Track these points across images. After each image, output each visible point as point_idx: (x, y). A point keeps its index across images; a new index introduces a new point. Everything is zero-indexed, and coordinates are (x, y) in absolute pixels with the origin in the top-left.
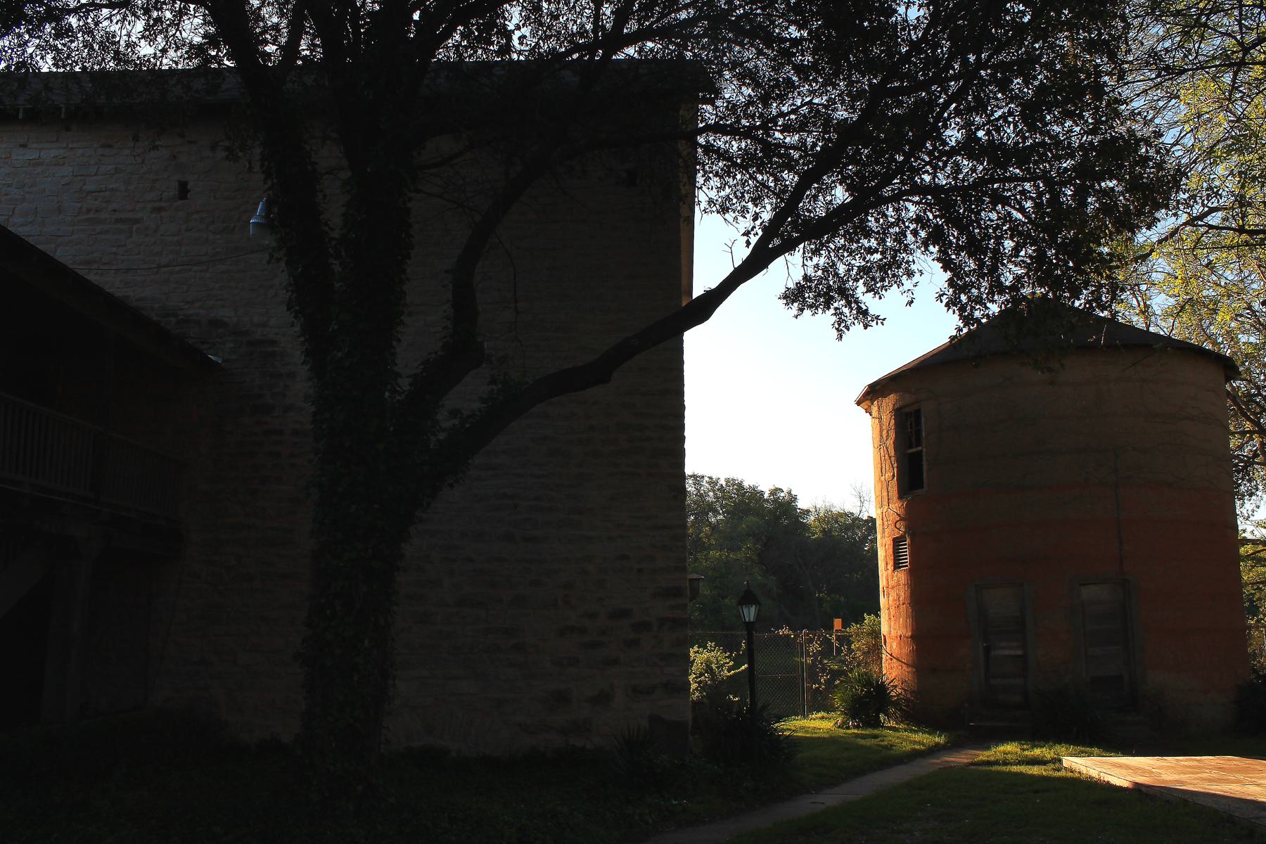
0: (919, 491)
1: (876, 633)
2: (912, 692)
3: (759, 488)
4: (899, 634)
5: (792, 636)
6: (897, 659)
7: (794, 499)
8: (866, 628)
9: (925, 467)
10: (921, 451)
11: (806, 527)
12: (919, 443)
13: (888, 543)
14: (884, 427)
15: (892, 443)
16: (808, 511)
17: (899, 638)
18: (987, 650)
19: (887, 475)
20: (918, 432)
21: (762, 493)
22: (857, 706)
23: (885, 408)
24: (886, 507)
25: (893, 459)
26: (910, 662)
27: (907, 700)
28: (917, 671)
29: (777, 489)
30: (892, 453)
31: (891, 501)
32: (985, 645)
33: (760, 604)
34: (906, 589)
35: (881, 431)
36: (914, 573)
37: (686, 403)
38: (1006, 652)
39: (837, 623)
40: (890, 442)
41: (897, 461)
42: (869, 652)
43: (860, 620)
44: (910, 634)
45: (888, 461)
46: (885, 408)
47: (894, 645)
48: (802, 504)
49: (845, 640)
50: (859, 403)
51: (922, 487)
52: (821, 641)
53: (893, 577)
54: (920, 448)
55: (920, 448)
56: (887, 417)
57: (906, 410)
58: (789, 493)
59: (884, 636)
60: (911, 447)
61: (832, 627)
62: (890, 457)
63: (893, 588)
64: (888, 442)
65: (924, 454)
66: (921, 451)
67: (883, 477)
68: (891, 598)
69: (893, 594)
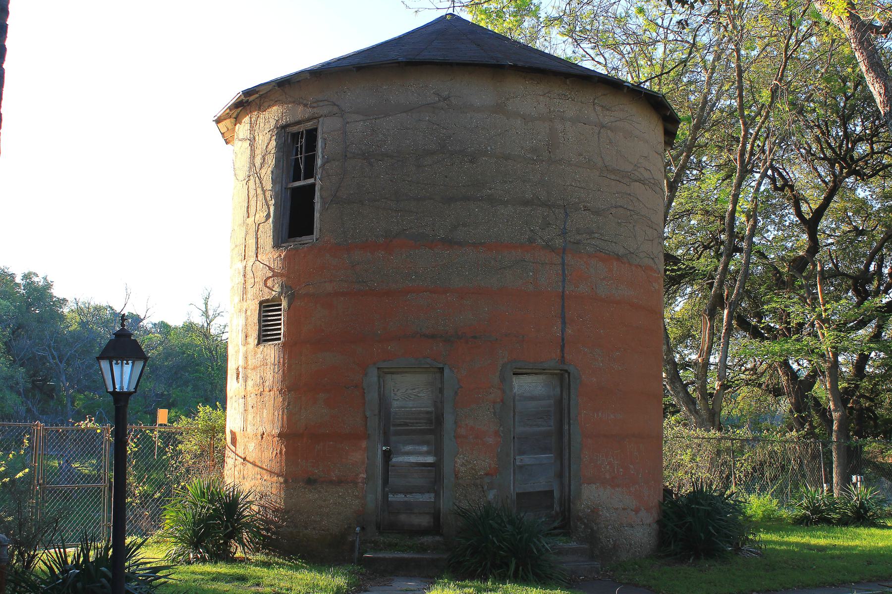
0: (306, 239)
1: (215, 431)
2: (276, 511)
3: (9, 270)
4: (260, 431)
5: (99, 431)
6: (254, 464)
7: (48, 286)
8: (201, 424)
9: (318, 206)
10: (313, 186)
11: (62, 317)
12: (310, 174)
13: (253, 307)
14: (258, 152)
15: (269, 172)
16: (65, 300)
17: (260, 438)
18: (387, 455)
19: (257, 216)
20: (310, 161)
21: (12, 276)
22: (429, 552)
23: (262, 125)
24: (253, 259)
25: (268, 194)
26: (276, 468)
27: (267, 522)
28: (286, 481)
29: (30, 274)
30: (268, 185)
31: (260, 251)
32: (384, 448)
33: (145, 358)
34: (276, 370)
35: (253, 156)
36: (291, 349)
37: (9, 10)
38: (413, 459)
39: (163, 415)
40: (267, 173)
41: (276, 196)
42: (202, 454)
43: (191, 413)
44: (278, 431)
45: (261, 197)
46: (262, 125)
47: (251, 446)
48: (57, 292)
49: (170, 438)
50: (218, 121)
51: (310, 232)
52: (138, 439)
53: (255, 353)
54: (311, 181)
55: (311, 181)
56: (266, 141)
57: (295, 129)
58: (45, 279)
59: (233, 434)
60: (297, 178)
61: (154, 421)
62: (264, 192)
63: (254, 369)
64: (263, 171)
65: (317, 188)
66: (313, 186)
67: (251, 219)
68: (250, 383)
69: (254, 378)
